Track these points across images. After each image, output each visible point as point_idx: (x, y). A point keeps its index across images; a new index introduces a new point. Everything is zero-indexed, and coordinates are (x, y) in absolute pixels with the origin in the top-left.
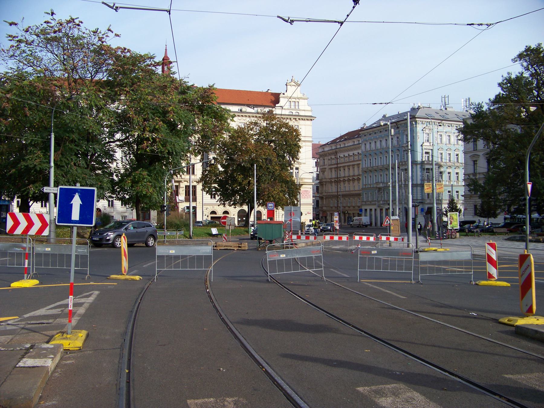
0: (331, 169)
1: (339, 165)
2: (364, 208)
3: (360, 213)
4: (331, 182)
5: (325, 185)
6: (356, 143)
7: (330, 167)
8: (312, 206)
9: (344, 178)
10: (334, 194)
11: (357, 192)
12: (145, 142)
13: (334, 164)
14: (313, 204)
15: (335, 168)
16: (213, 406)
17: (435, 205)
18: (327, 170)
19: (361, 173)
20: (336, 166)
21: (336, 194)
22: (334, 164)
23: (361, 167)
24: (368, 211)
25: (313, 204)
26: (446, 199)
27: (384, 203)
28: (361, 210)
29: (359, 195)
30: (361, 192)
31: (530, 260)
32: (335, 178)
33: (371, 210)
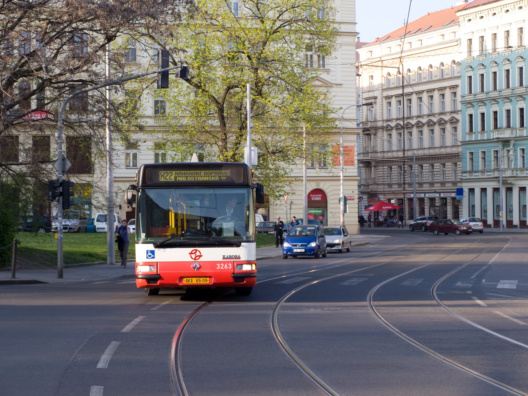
0: (388, 97)
1: (407, 90)
2: (466, 187)
3: (458, 197)
4: (388, 129)
5: (375, 135)
6: (447, 39)
7: (385, 94)
8: (356, 183)
9: (455, 115)
10: (395, 154)
11: (449, 150)
12: (25, 204)
13: (396, 88)
14: (359, 178)
15: (397, 96)
16: (2, 101)
17: (341, 187)
18: (379, 101)
19: (459, 107)
20: (400, 91)
21: (400, 154)
22: (396, 88)
23: (459, 94)
24: (477, 192)
25: (359, 178)
26: (406, 179)
27: (515, 175)
28: (460, 192)
29: (455, 158)
30: (460, 149)
31: (494, 256)
32: (398, 119)
33: (484, 190)
